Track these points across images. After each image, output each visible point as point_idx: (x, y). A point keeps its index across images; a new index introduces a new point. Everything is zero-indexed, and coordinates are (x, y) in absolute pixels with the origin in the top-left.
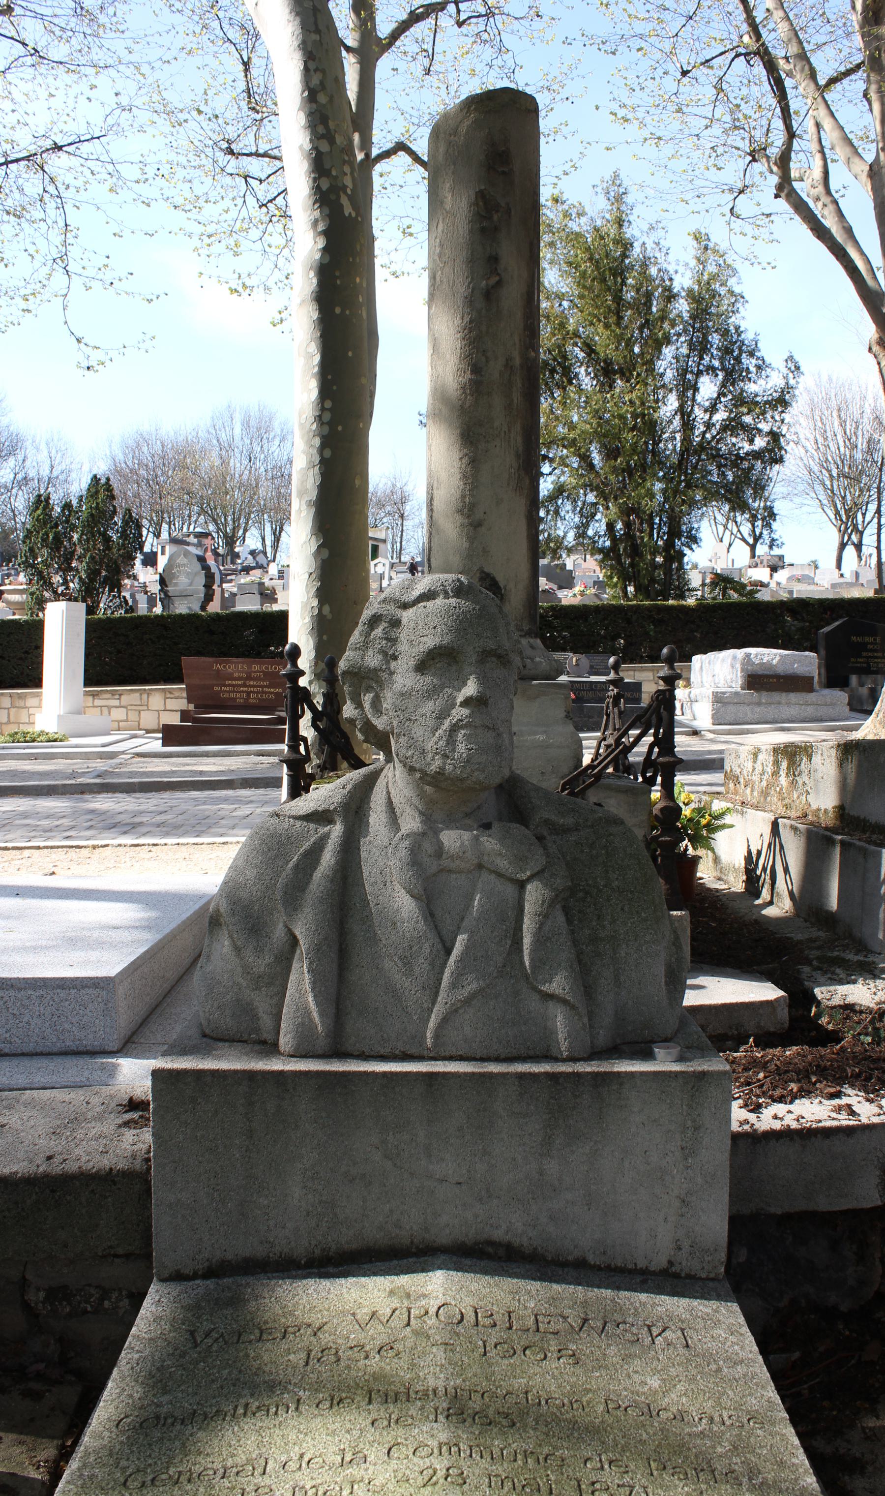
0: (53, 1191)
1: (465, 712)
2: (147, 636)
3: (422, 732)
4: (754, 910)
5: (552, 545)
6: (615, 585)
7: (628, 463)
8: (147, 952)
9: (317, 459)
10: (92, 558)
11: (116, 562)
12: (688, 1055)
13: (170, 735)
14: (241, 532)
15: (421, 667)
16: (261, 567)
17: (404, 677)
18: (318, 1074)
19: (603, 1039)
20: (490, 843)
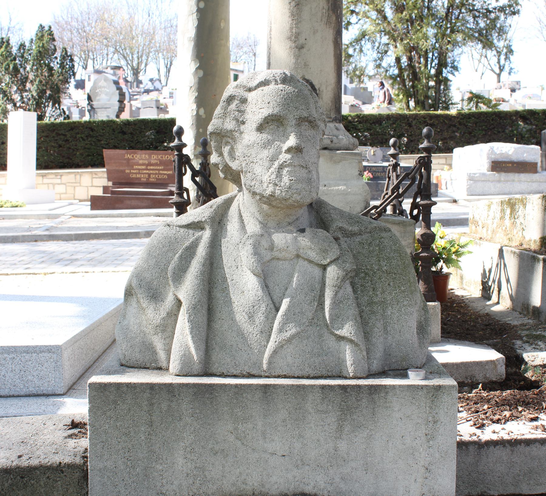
0: (22, 477)
1: (288, 156)
2: (79, 136)
3: (260, 170)
4: (487, 308)
5: (357, 73)
6: (401, 101)
7: (410, 15)
8: (83, 331)
9: (195, 9)
10: (41, 82)
11: (57, 85)
12: (431, 376)
13: (97, 203)
14: (143, 66)
15: (260, 128)
16: (157, 90)
17: (250, 136)
18: (195, 385)
19: (376, 366)
20: (304, 241)
